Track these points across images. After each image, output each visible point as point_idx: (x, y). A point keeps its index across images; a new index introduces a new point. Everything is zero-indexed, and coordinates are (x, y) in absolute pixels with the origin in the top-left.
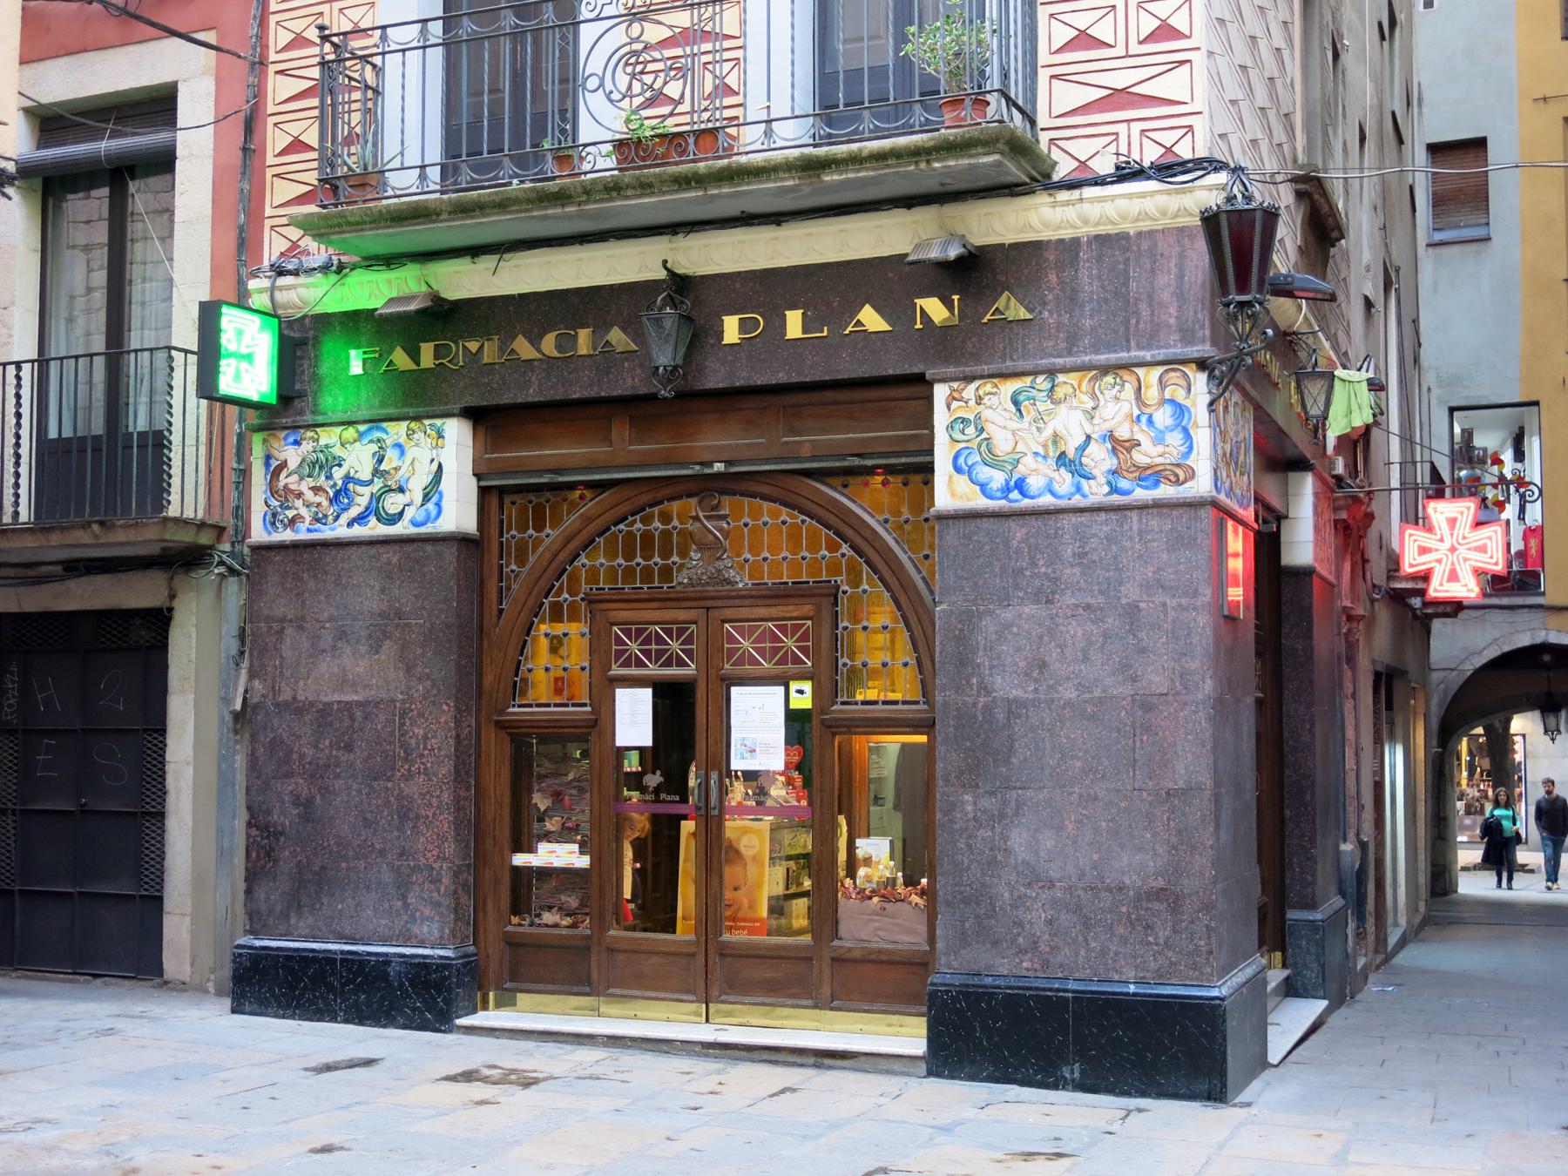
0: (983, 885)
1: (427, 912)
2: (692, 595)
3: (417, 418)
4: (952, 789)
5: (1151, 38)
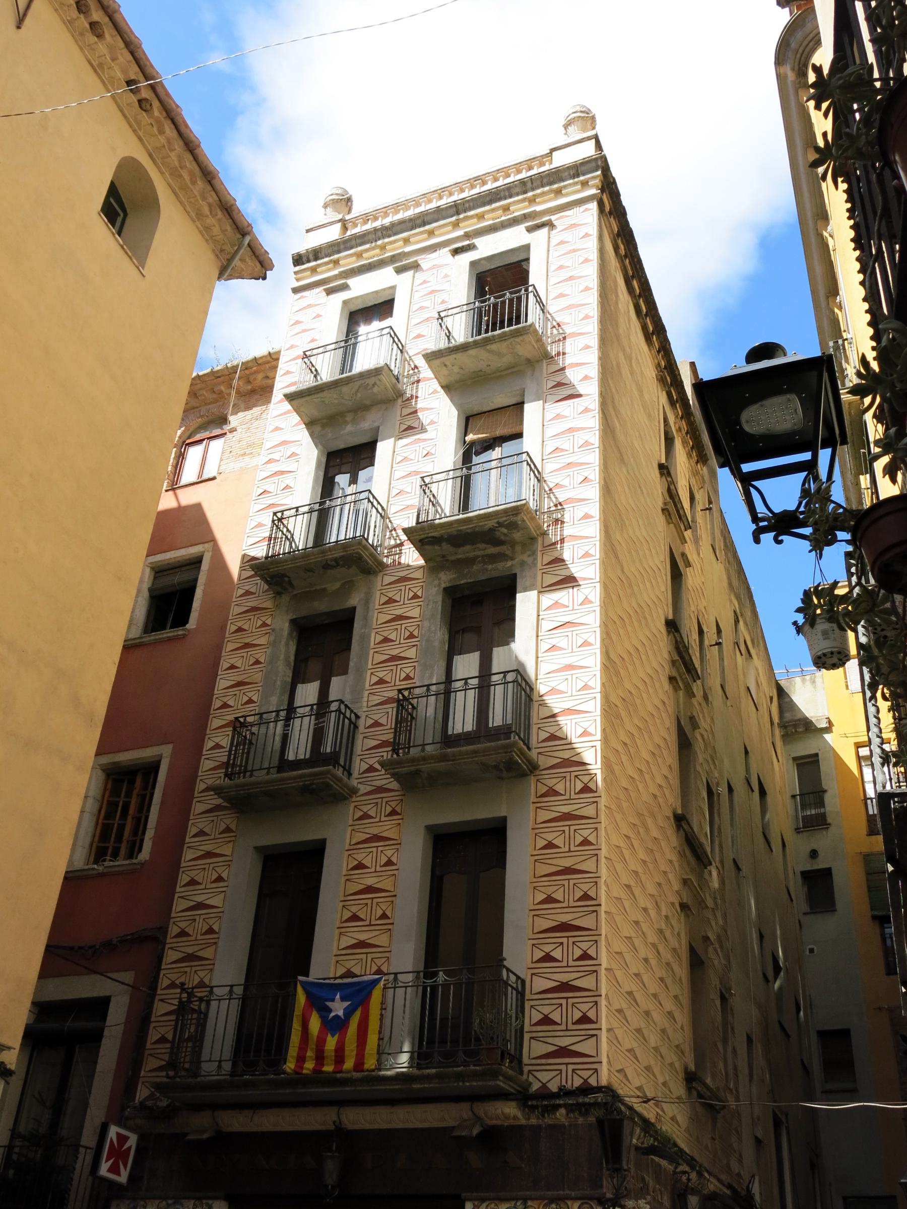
5: (579, 959)
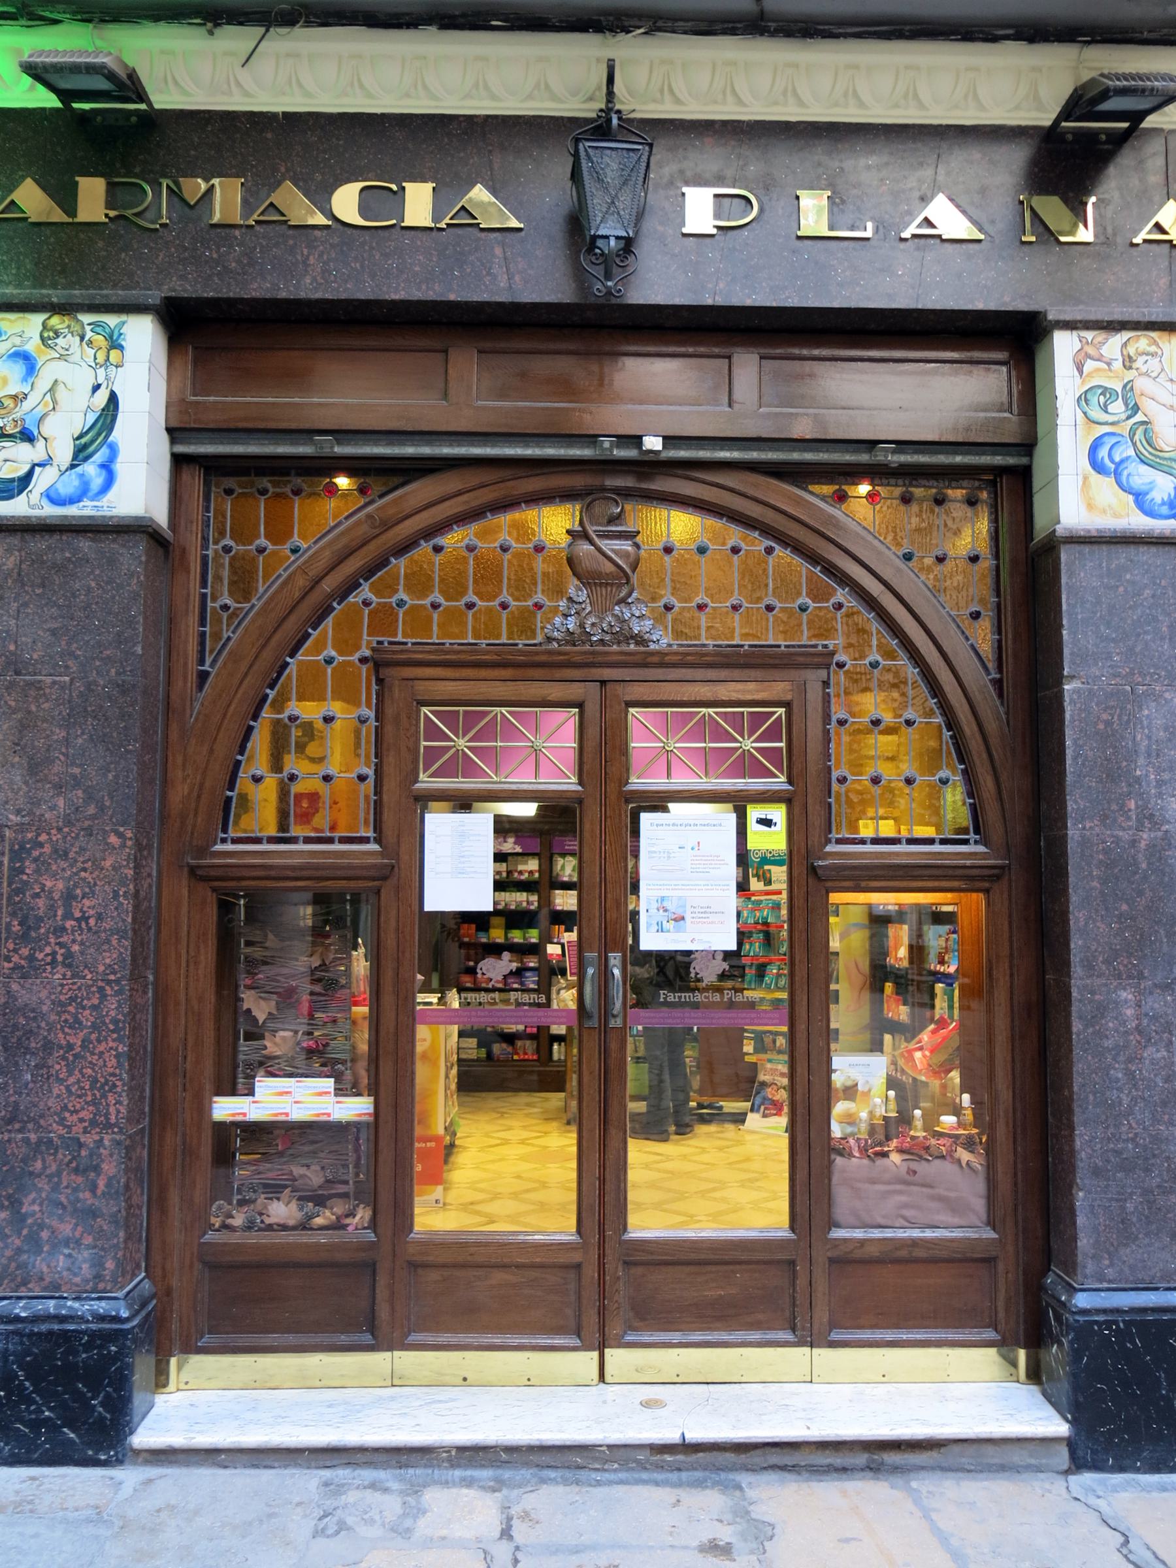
0: (1157, 1139)
1: (66, 1229)
2: (578, 659)
3: (65, 309)
4: (1099, 981)
